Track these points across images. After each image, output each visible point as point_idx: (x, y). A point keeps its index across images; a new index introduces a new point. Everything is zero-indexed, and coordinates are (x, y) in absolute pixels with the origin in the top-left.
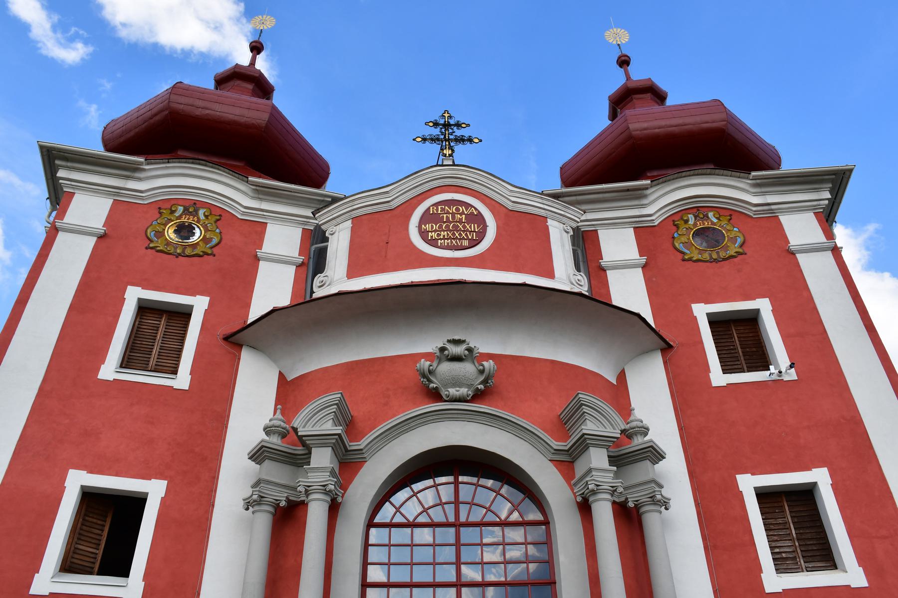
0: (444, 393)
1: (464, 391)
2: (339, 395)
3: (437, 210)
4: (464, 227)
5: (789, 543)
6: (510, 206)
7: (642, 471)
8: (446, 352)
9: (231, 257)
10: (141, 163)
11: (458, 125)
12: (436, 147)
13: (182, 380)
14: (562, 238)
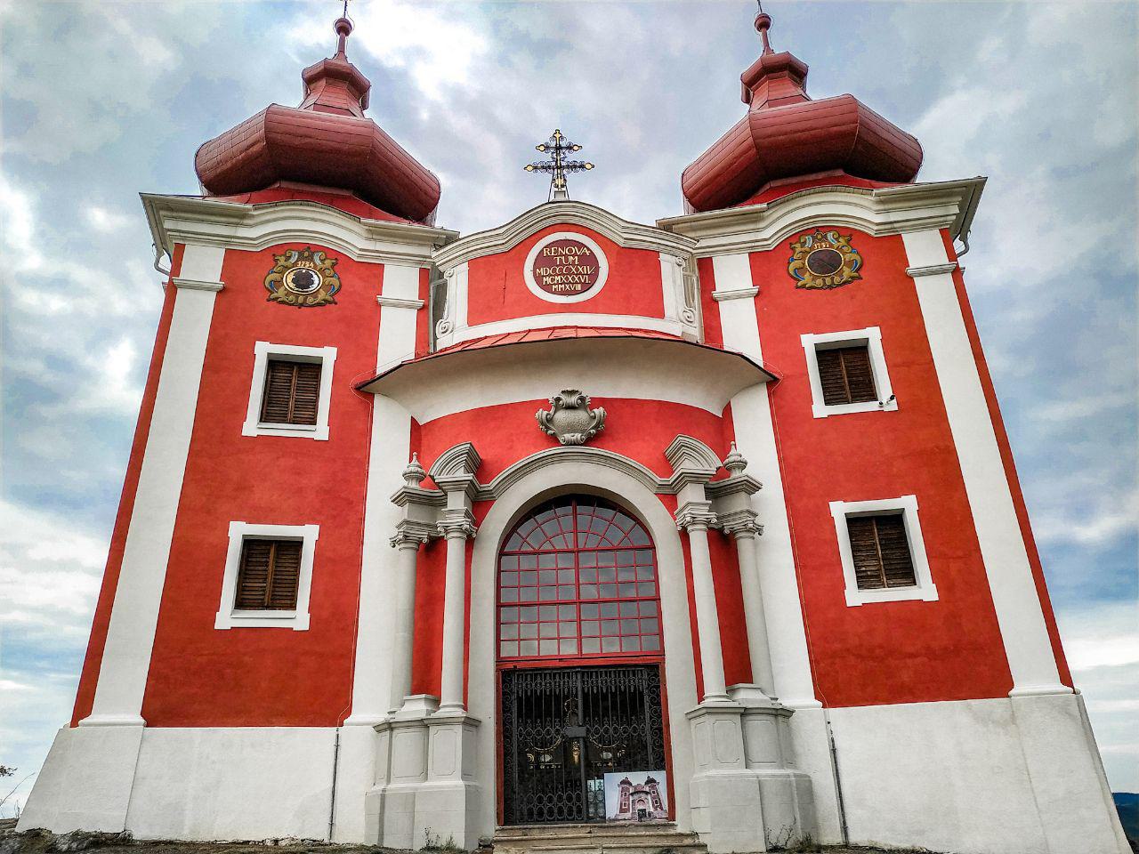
0: (561, 439)
1: (578, 436)
2: (469, 445)
3: (551, 252)
4: (577, 270)
5: (875, 563)
6: (621, 242)
7: (739, 503)
8: (561, 402)
9: (350, 302)
10: (249, 210)
11: (570, 148)
12: (548, 176)
13: (321, 431)
14: (673, 273)
